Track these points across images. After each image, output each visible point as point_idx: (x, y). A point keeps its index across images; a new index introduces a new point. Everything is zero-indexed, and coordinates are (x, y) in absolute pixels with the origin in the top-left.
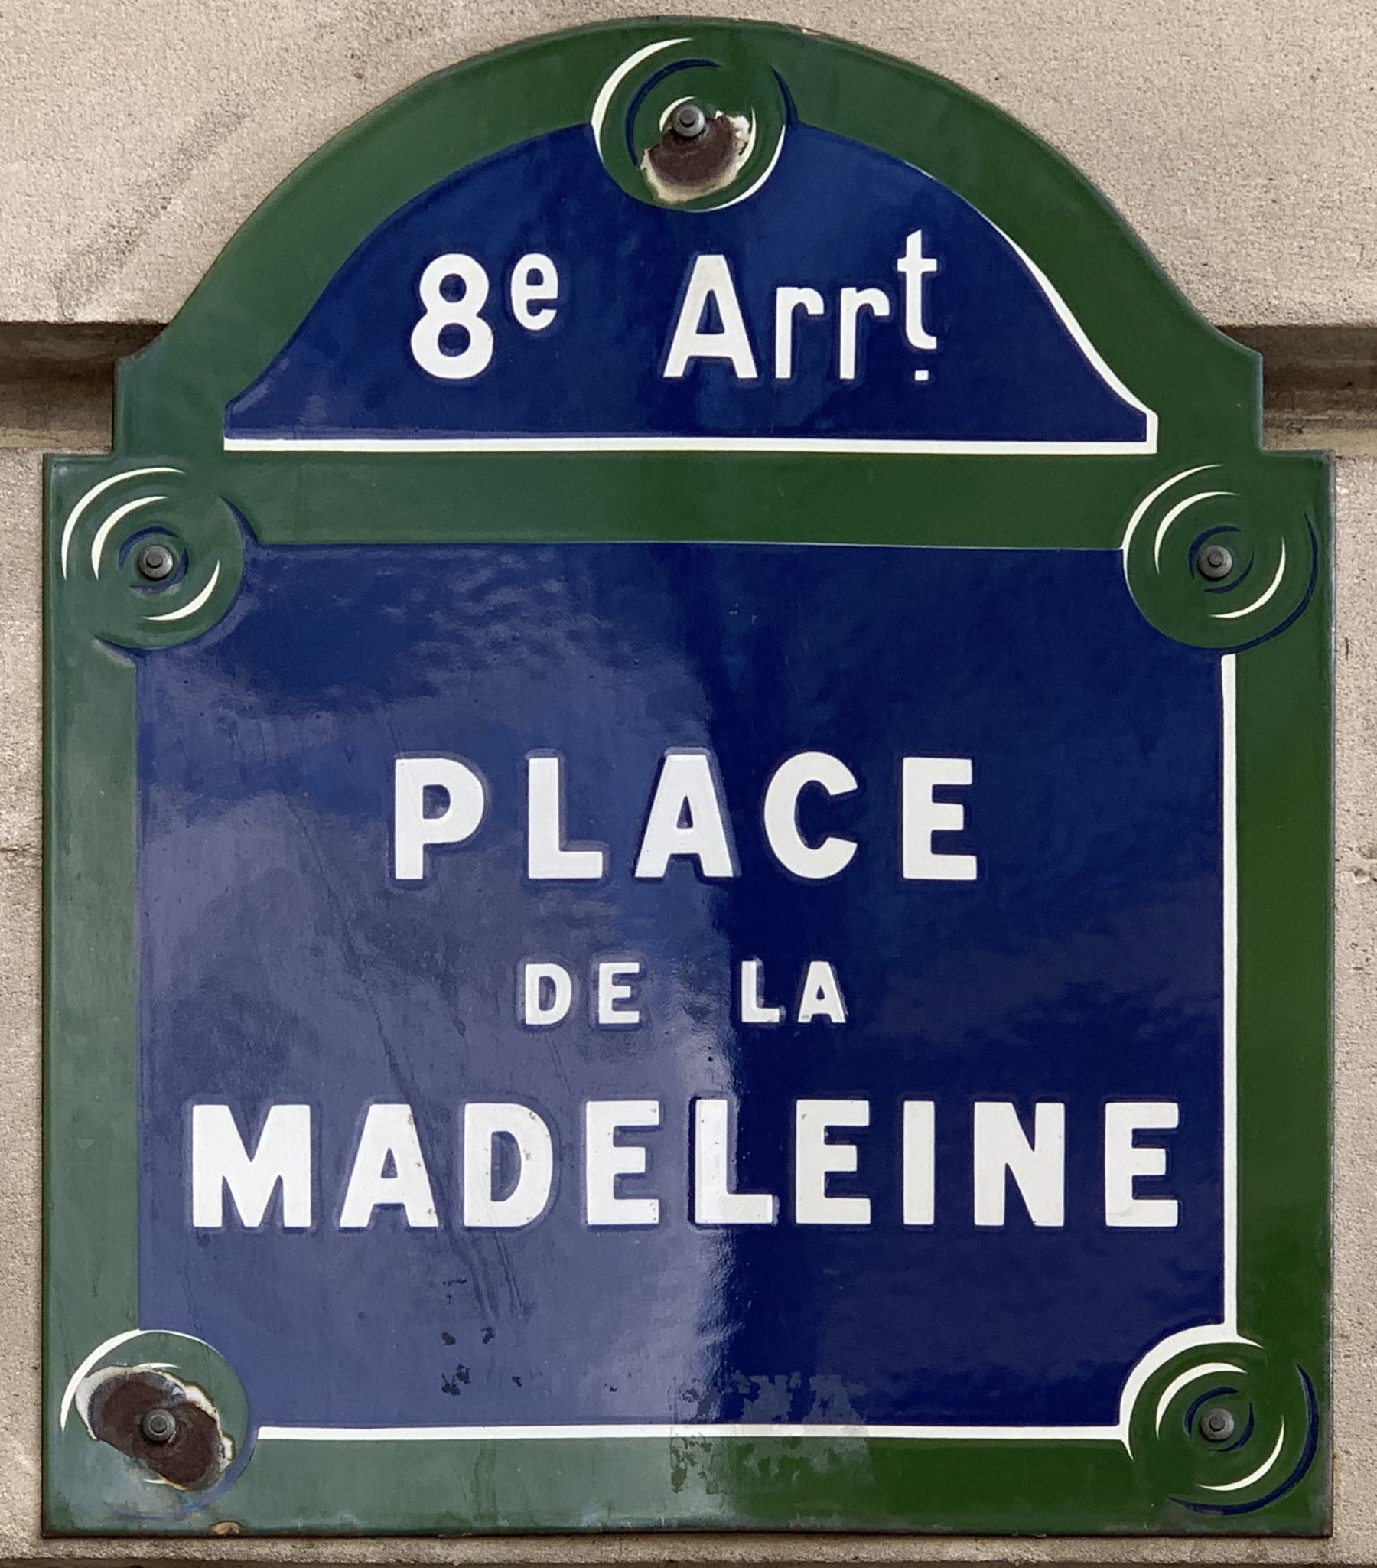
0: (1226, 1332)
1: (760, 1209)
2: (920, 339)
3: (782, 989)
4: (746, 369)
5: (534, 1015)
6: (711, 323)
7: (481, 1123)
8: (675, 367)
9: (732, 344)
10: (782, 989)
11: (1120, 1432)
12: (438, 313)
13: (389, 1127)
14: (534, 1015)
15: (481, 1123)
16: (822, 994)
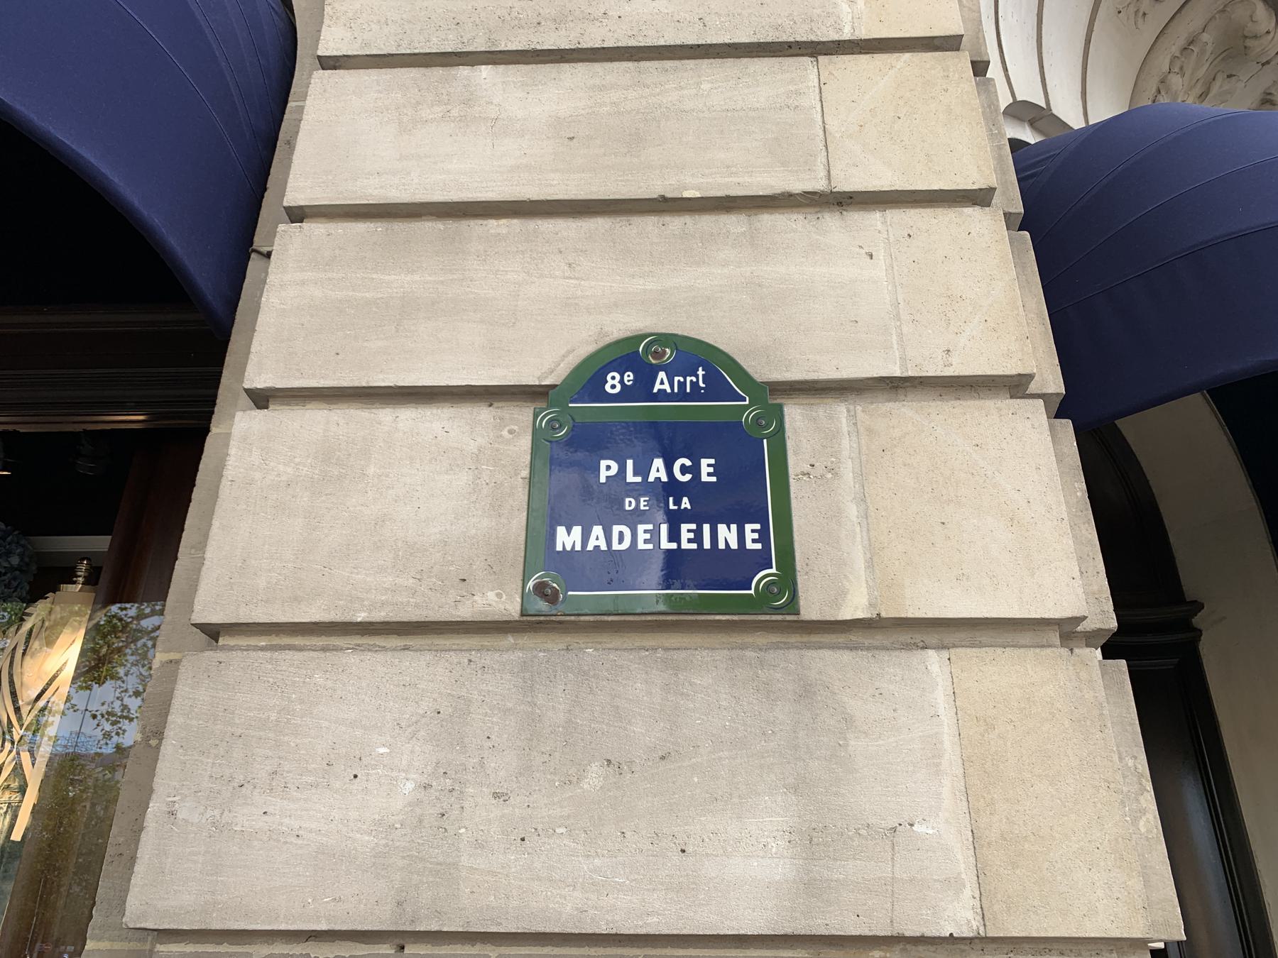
0: (773, 570)
1: (674, 546)
2: (702, 385)
3: (677, 502)
4: (669, 390)
5: (627, 508)
6: (662, 383)
7: (616, 529)
8: (655, 391)
9: (667, 387)
10: (677, 502)
11: (752, 592)
12: (610, 382)
13: (598, 530)
14: (627, 508)
15: (616, 529)
16: (686, 503)
